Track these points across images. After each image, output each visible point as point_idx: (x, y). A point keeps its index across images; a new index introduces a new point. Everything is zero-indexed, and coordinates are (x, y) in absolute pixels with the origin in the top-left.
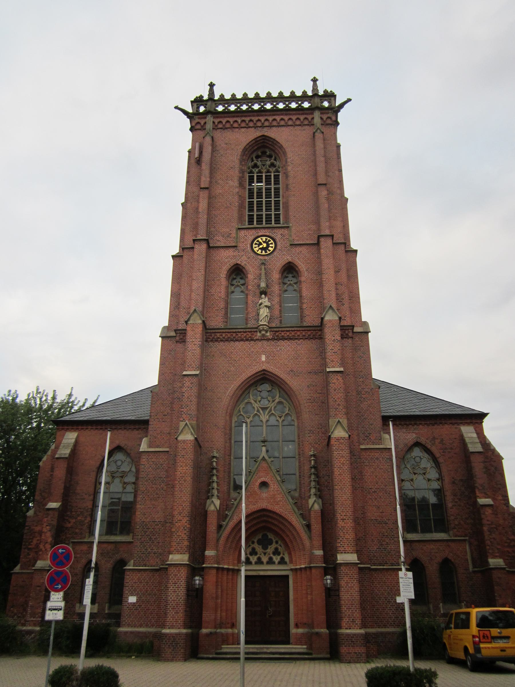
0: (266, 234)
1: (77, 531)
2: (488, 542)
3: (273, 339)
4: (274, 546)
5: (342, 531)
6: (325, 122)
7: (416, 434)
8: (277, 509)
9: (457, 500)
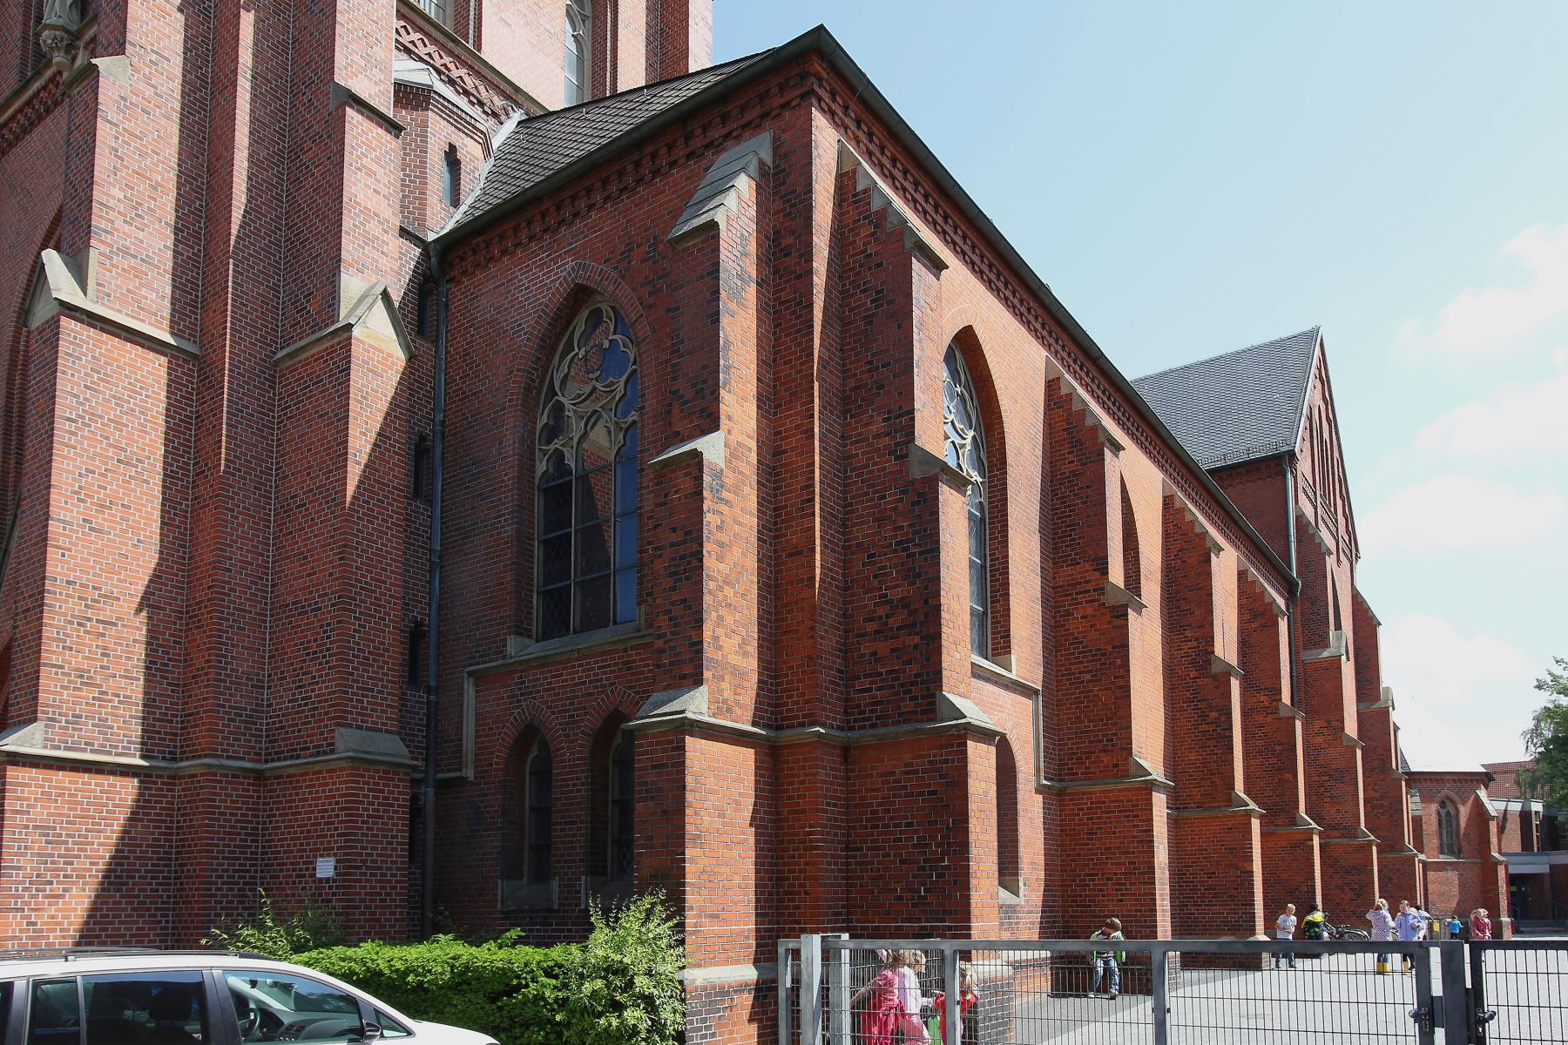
7: (575, 253)
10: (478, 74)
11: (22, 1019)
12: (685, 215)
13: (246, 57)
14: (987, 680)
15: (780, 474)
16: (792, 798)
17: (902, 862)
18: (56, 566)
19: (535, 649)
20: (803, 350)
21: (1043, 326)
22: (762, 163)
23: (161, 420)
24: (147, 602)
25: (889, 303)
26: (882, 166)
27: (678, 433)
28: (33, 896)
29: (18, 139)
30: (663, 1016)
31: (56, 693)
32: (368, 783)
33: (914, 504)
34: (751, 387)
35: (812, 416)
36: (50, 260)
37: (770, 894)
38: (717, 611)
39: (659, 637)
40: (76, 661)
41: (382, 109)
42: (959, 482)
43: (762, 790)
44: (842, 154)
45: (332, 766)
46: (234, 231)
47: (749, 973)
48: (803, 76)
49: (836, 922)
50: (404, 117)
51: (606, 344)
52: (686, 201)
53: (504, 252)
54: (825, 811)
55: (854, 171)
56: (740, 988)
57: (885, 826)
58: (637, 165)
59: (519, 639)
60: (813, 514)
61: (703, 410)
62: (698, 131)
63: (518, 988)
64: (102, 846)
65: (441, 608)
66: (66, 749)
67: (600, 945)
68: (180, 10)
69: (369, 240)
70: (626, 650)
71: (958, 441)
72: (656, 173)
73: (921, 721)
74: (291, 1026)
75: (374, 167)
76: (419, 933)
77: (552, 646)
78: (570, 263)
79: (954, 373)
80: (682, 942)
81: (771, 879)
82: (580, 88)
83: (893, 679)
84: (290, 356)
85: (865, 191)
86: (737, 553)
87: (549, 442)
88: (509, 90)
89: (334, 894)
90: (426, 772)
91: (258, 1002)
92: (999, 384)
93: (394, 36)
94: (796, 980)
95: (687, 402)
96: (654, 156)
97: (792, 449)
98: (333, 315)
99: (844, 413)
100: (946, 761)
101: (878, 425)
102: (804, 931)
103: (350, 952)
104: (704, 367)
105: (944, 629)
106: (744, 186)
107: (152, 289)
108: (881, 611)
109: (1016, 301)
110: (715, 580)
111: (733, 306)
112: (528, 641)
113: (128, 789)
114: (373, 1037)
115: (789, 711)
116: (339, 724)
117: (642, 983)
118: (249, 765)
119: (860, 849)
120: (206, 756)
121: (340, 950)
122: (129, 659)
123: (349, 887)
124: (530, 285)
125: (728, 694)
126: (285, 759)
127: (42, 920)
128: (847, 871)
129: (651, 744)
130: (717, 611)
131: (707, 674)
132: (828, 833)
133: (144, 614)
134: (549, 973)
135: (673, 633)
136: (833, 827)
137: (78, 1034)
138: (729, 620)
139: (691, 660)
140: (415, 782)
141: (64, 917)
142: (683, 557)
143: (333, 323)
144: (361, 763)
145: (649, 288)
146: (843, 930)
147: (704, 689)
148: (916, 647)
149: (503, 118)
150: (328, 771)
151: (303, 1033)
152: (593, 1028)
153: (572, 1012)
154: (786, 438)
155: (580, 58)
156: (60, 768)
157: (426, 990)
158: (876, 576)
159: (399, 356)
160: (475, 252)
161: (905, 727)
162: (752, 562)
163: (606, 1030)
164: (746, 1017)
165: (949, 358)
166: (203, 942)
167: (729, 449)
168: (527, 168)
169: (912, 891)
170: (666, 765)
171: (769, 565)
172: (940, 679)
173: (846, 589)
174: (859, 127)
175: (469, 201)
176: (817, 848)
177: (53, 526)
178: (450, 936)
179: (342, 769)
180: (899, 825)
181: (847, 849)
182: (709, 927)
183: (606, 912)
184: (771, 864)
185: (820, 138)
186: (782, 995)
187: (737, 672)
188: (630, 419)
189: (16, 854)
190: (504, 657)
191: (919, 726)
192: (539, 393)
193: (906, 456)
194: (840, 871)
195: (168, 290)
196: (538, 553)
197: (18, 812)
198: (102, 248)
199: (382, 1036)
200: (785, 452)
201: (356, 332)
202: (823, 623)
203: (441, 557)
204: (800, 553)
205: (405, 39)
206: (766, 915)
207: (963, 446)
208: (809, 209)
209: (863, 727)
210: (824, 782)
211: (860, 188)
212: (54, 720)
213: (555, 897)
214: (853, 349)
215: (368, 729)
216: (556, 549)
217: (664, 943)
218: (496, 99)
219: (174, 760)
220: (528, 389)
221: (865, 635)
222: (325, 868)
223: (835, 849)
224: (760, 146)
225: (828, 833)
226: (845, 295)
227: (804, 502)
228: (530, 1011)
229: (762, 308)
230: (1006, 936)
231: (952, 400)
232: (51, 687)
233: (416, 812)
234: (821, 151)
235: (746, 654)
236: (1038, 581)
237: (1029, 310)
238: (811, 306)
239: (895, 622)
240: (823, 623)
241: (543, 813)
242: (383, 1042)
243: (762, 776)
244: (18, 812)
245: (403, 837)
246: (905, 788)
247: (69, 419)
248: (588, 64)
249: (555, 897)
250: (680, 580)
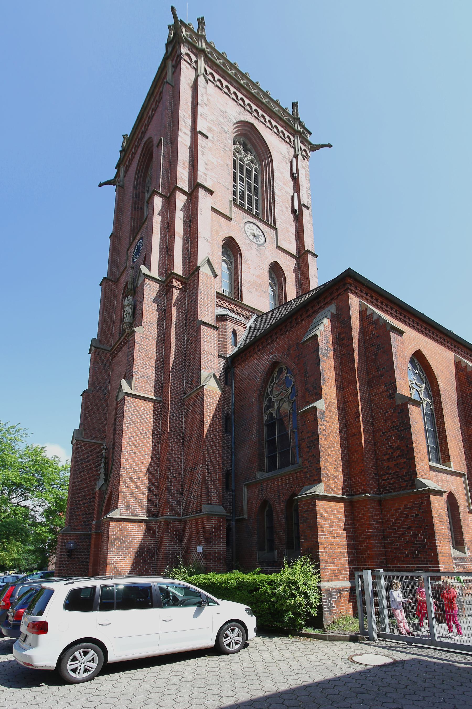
7: (273, 353)
10: (242, 308)
11: (98, 598)
12: (306, 334)
13: (174, 318)
14: (441, 472)
15: (346, 409)
16: (359, 520)
17: (407, 542)
18: (124, 464)
19: (266, 475)
20: (351, 369)
21: (451, 345)
22: (332, 314)
23: (152, 420)
24: (148, 472)
25: (382, 348)
26: (377, 305)
27: (308, 402)
28: (116, 560)
29: (118, 353)
30: (311, 599)
31: (123, 500)
32: (212, 521)
33: (399, 413)
34: (334, 383)
35: (357, 389)
36: (123, 382)
37: (354, 555)
38: (325, 457)
39: (305, 468)
40: (129, 490)
41: (212, 324)
42: (417, 403)
43: (347, 517)
44: (361, 305)
45: (201, 517)
46: (171, 365)
47: (347, 584)
48: (344, 285)
49: (382, 565)
50: (220, 324)
51: (284, 378)
52: (307, 329)
53: (250, 356)
54: (373, 524)
55: (366, 309)
56: (344, 589)
57: (398, 529)
58: (291, 323)
59: (260, 472)
60: (360, 421)
61: (316, 393)
62: (310, 309)
63: (259, 589)
64: (136, 544)
65: (235, 465)
66: (126, 516)
67: (285, 574)
68: (157, 311)
69: (209, 360)
70: (296, 473)
71: (418, 389)
72: (297, 324)
73: (410, 489)
74: (181, 601)
75: (210, 340)
76: (229, 570)
77: (271, 474)
78: (271, 355)
79: (415, 367)
80: (319, 572)
81: (353, 549)
82: (275, 304)
83: (396, 475)
84: (187, 397)
85: (370, 314)
86: (332, 437)
87: (267, 410)
88: (252, 310)
89: (203, 557)
90: (232, 517)
91: (173, 593)
92: (433, 367)
93: (215, 303)
94: (363, 587)
96: (296, 319)
97: (350, 401)
98: (199, 384)
99: (369, 386)
100: (422, 503)
101: (383, 388)
102: (364, 568)
103: (205, 576)
104: (316, 380)
105: (415, 455)
106: (326, 322)
107: (149, 385)
108: (390, 451)
109: (438, 338)
110: (324, 447)
111: (325, 359)
112: (263, 473)
113: (143, 527)
114: (205, 605)
115: (356, 489)
116: (203, 504)
117: (302, 588)
118: (177, 518)
119: (389, 537)
120: (165, 516)
121: (203, 576)
122: (143, 488)
123: (207, 555)
124: (260, 364)
125: (331, 485)
127: (119, 566)
128: (385, 546)
129: (304, 504)
130: (325, 457)
131: (323, 479)
132: (375, 532)
133: (147, 475)
134: (269, 584)
135: (310, 466)
136: (377, 529)
137: (114, 603)
138: (330, 460)
139: (317, 475)
140: (227, 520)
141: (139, 565)
142: (311, 441)
144: (210, 515)
145: (297, 358)
146: (381, 568)
147: (322, 484)
148: (404, 463)
149: (250, 318)
150: (200, 518)
151: (185, 603)
152: (285, 604)
153: (278, 597)
154: (347, 398)
155: (274, 296)
156: (124, 522)
157: (229, 589)
158: (386, 440)
159: (219, 392)
160: (242, 358)
161: (403, 492)
162: (338, 440)
163: (290, 604)
164: (347, 601)
165: (412, 361)
166: (162, 573)
167: (327, 404)
168: (257, 331)
169: (412, 553)
170: (309, 511)
171: (344, 440)
172: (416, 474)
173: (375, 445)
174: (367, 295)
175: (240, 344)
176: (371, 537)
177: (123, 453)
178: (238, 571)
179: (204, 518)
180: (404, 528)
181: (384, 537)
182: (329, 567)
183: (289, 562)
184: (353, 544)
185: (352, 302)
186: (358, 593)
187: (334, 477)
188: (293, 399)
189: (112, 547)
190: (256, 479)
191: (408, 491)
192: (263, 396)
193: (394, 397)
194: (382, 546)
195: (154, 384)
196: (265, 444)
197: (112, 535)
198: (137, 377)
199: (208, 605)
200: (348, 402)
201: (205, 387)
202: (367, 458)
203: (235, 449)
204: (356, 435)
205: (219, 303)
206: (353, 562)
207: (421, 390)
208: (350, 324)
209: (386, 493)
210: (372, 513)
211: (368, 314)
212: (123, 508)
213: (276, 557)
214: (371, 365)
215: (212, 504)
216: (271, 443)
217: (310, 573)
218: (248, 313)
219: (156, 517)
220: (260, 395)
221: (384, 460)
222: (200, 549)
223: (379, 538)
224: (332, 308)
225: (375, 532)
226: (366, 348)
227: (356, 418)
228: (263, 597)
229: (335, 358)
230: (461, 570)
231: (415, 376)
232: (122, 498)
233: (229, 530)
234: (353, 305)
235: (337, 471)
236: (460, 434)
237: (444, 340)
238: (353, 354)
239: (395, 454)
240: (367, 458)
241: (271, 528)
242: (209, 607)
243: (347, 512)
244: (112, 535)
245: (224, 538)
246: (405, 514)
247: (127, 423)
248: (277, 297)
249: (276, 557)
250: (311, 448)
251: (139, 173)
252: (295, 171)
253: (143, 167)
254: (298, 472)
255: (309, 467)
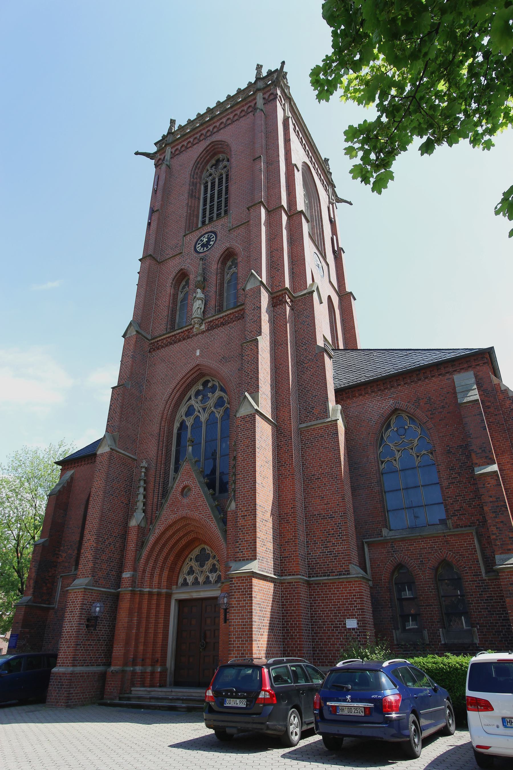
0: (208, 231)
1: (66, 564)
2: (493, 529)
3: (208, 330)
4: (211, 562)
5: (242, 531)
6: (267, 100)
7: (394, 399)
8: (196, 515)
9: (456, 475)
61: (486, 457)
70: (445, 536)
95: (478, 453)
126: (321, 576)
142: (497, 507)
143: (327, 418)
150: (339, 583)
190: (382, 536)
251: (198, 164)
252: (332, 216)
253: (203, 161)
254: (448, 536)
255: (498, 535)
